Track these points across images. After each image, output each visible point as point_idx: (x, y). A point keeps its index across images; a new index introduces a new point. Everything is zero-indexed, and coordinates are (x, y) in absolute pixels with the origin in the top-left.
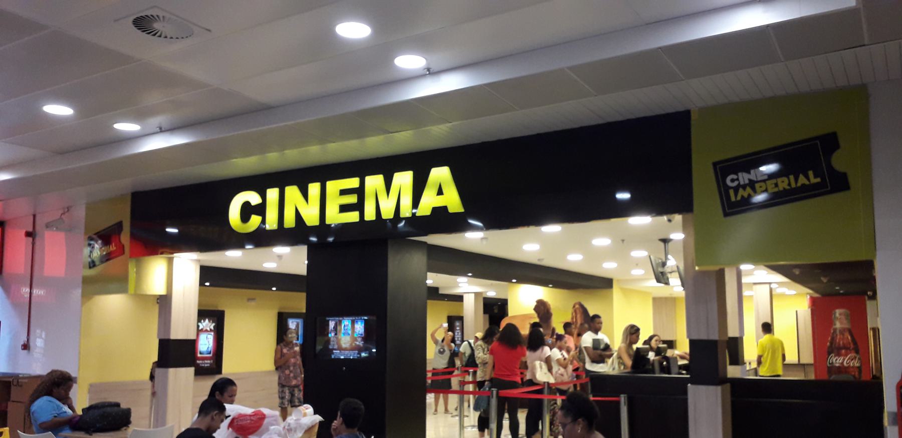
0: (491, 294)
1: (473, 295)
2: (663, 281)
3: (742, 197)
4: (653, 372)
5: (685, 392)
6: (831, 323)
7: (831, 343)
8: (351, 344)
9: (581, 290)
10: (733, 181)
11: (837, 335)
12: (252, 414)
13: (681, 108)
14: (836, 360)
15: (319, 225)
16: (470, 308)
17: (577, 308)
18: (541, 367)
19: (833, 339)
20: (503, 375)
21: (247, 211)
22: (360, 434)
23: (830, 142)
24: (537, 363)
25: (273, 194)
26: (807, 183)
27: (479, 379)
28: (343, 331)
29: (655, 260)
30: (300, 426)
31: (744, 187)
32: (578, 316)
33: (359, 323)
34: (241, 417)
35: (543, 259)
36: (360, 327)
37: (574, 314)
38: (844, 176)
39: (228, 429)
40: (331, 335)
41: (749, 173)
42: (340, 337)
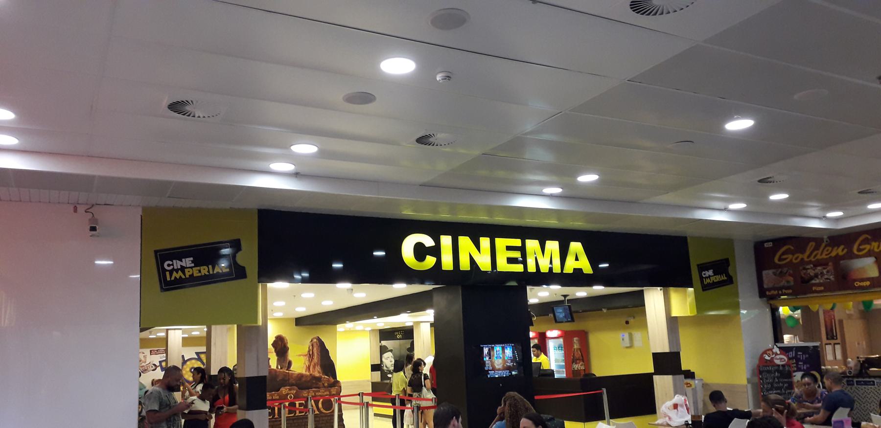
3: (175, 277)
8: (503, 366)
10: (169, 265)
13: (683, 235)
15: (879, 276)
21: (420, 251)
28: (495, 356)
31: (177, 271)
32: (315, 349)
33: (508, 349)
36: (509, 352)
37: (311, 348)
38: (243, 268)
40: (486, 359)
41: (181, 266)
42: (493, 360)
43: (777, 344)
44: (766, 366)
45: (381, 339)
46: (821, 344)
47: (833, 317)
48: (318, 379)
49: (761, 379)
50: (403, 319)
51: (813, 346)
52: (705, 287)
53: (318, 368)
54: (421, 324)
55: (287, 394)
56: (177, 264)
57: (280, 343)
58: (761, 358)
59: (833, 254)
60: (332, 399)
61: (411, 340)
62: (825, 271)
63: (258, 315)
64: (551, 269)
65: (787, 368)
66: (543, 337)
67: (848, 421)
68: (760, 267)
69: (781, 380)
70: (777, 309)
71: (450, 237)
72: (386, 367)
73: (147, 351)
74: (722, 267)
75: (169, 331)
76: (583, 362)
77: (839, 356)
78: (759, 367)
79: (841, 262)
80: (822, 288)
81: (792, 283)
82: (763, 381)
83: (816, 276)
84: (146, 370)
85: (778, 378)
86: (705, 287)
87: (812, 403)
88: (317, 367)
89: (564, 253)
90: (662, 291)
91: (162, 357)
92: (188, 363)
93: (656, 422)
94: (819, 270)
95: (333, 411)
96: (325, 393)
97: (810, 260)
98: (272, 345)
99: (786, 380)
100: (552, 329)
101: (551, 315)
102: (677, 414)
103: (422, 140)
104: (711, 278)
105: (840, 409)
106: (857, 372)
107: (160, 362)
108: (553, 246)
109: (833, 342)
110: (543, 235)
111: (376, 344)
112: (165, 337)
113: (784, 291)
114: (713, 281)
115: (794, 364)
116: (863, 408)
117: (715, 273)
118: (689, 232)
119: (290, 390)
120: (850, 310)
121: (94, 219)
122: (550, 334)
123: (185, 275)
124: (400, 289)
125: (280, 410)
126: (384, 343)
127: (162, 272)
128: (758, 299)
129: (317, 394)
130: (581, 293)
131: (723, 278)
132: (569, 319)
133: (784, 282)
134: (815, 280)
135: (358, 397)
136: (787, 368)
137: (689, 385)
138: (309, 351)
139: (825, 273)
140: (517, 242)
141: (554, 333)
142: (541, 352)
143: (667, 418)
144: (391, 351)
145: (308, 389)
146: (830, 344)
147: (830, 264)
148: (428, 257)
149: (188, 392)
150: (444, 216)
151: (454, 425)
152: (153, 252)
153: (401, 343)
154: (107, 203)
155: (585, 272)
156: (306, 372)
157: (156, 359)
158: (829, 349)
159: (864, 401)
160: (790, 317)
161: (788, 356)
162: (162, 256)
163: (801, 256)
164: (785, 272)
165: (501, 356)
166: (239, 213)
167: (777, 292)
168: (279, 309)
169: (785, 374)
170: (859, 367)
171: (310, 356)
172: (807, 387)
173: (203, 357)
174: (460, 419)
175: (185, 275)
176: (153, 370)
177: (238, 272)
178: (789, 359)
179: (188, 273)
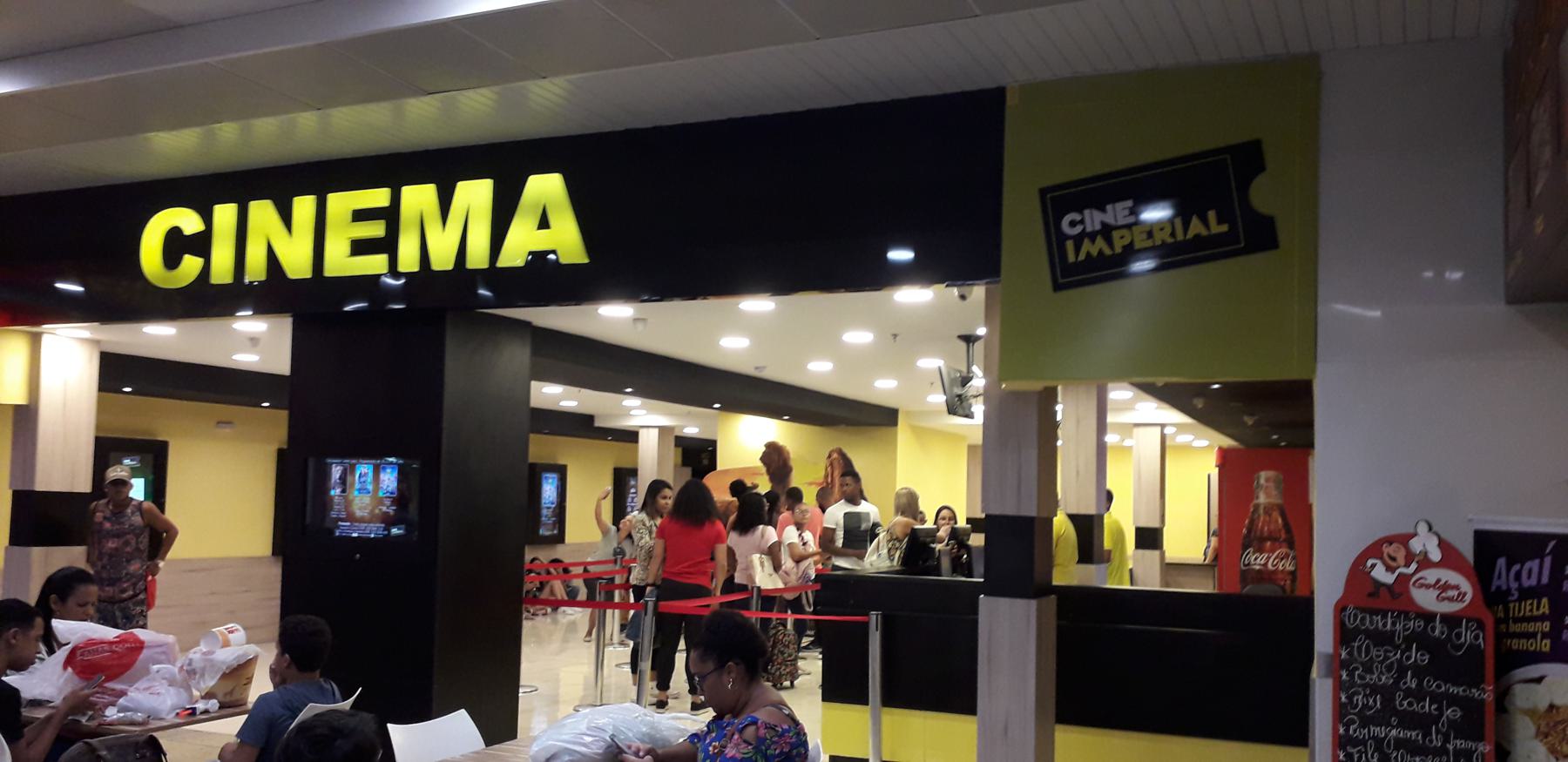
0: (691, 431)
1: (657, 430)
2: (961, 412)
3: (1088, 254)
4: (937, 570)
5: (974, 609)
6: (1251, 494)
7: (1249, 531)
8: (372, 511)
9: (843, 427)
10: (1073, 224)
11: (1259, 516)
12: (115, 640)
13: (989, 84)
14: (1256, 559)
16: (652, 459)
18: (762, 564)
19: (1252, 522)
20: (680, 574)
21: (176, 246)
22: (325, 681)
23: (1249, 158)
24: (756, 558)
25: (225, 214)
26: (1204, 232)
27: (633, 581)
28: (357, 486)
29: (949, 374)
30: (212, 664)
31: (1092, 237)
33: (389, 470)
34: (91, 644)
35: (764, 367)
36: (389, 479)
39: (65, 668)
40: (335, 492)
41: (1103, 210)
42: (351, 497)
56: (1093, 219)
69: (1433, 685)
78: (1344, 609)
82: (1351, 674)
85: (1419, 672)
98: (761, 459)
99: (1453, 690)
115: (1542, 618)
140: (378, 197)
165: (370, 487)
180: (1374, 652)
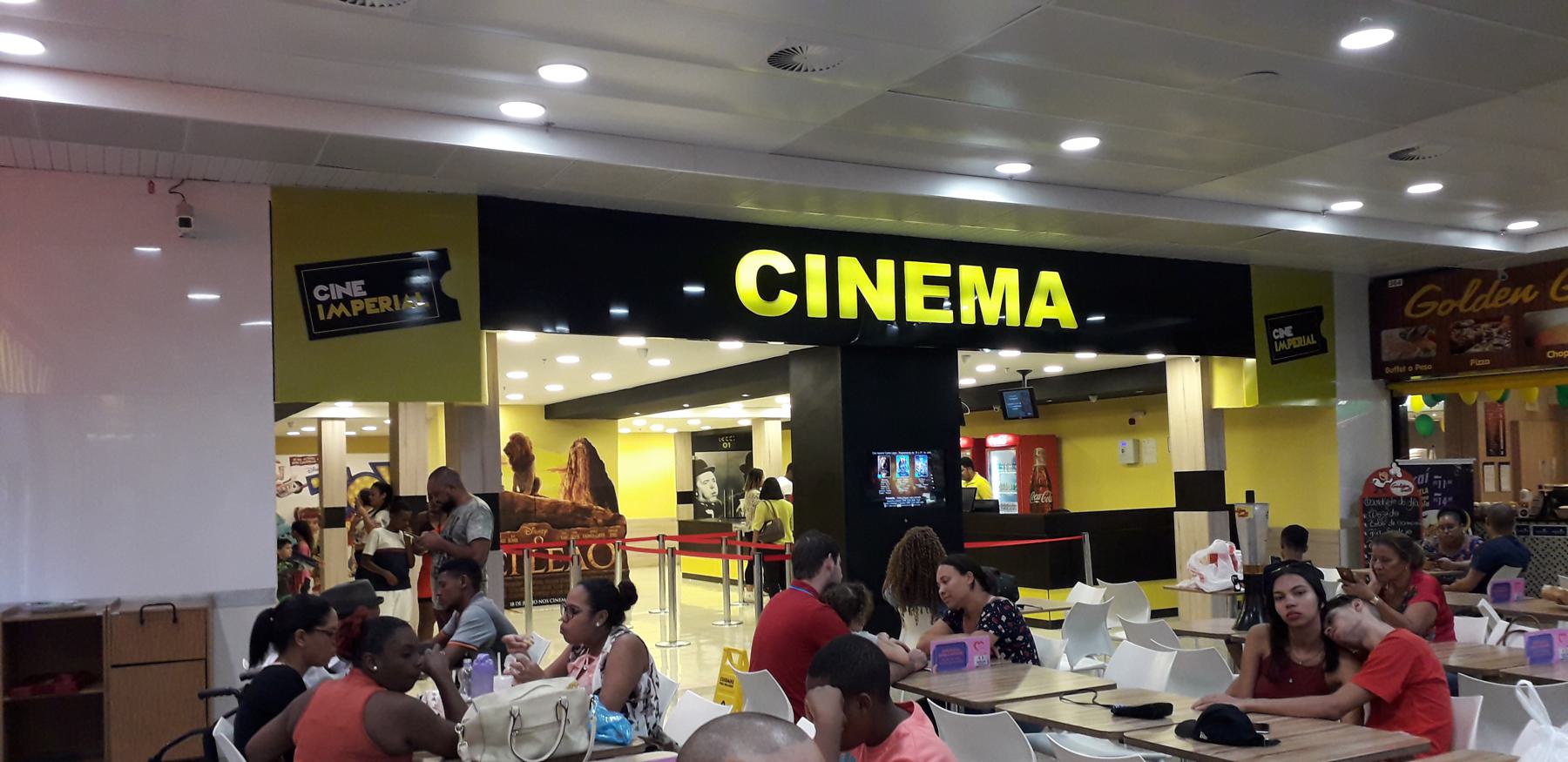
3: (334, 315)
8: (911, 488)
10: (322, 293)
17: (579, 448)
19: (1034, 477)
21: (769, 283)
28: (898, 471)
31: (336, 303)
32: (580, 460)
33: (921, 459)
36: (922, 464)
37: (573, 457)
38: (454, 303)
41: (344, 286)
42: (894, 479)
43: (1397, 460)
44: (1376, 499)
45: (695, 449)
46: (1477, 463)
47: (1501, 416)
48: (588, 511)
49: (1365, 521)
50: (732, 413)
51: (1463, 466)
52: (1278, 357)
53: (586, 493)
54: (766, 422)
55: (533, 536)
56: (337, 291)
57: (519, 449)
58: (1369, 483)
59: (1513, 300)
60: (611, 546)
61: (748, 452)
62: (1495, 331)
63: (483, 394)
64: (1002, 322)
65: (1412, 503)
66: (980, 447)
67: (1518, 583)
68: (1378, 322)
70: (1403, 400)
71: (822, 258)
72: (704, 496)
73: (284, 459)
74: (1309, 321)
75: (323, 422)
76: (1050, 490)
77: (1506, 486)
78: (1364, 499)
79: (1527, 314)
80: (1488, 362)
81: (1433, 353)
83: (1479, 339)
84: (284, 492)
85: (1395, 519)
86: (1278, 357)
87: (1454, 559)
88: (583, 491)
89: (1027, 290)
90: (1199, 363)
91: (312, 469)
92: (358, 481)
93: (1178, 586)
94: (1484, 329)
95: (614, 566)
96: (599, 536)
97: (1470, 312)
100: (996, 434)
101: (997, 408)
102: (1216, 570)
103: (780, 60)
104: (1289, 340)
105: (1505, 569)
106: (1537, 512)
107: (309, 479)
108: (1008, 277)
109: (1497, 459)
110: (990, 257)
111: (687, 458)
112: (316, 434)
113: (1418, 367)
114: (1292, 347)
115: (1426, 495)
116: (1542, 575)
117: (1296, 333)
118: (1254, 255)
119: (537, 528)
120: (1532, 405)
121: (184, 206)
122: (992, 441)
123: (351, 313)
124: (732, 351)
125: (520, 560)
126: (699, 456)
127: (310, 304)
128: (1370, 381)
129: (586, 536)
130: (1053, 366)
131: (1309, 342)
132: (1029, 414)
133: (1419, 350)
134: (1476, 348)
135: (657, 542)
136: (1412, 503)
137: (1243, 513)
138: (570, 464)
139: (1495, 335)
140: (944, 270)
141: (1001, 440)
142: (974, 470)
143: (1198, 578)
144: (712, 469)
145: (569, 527)
146: (1492, 463)
147: (1506, 318)
148: (783, 293)
149: (362, 522)
150: (813, 217)
151: (829, 568)
152: (294, 269)
153: (729, 457)
154: (206, 178)
155: (1063, 326)
156: (565, 498)
157: (302, 473)
158: (1489, 471)
159: (1544, 562)
160: (1424, 417)
161: (1415, 483)
162: (310, 276)
163: (1453, 304)
164: (1422, 332)
165: (908, 471)
166: (444, 201)
167: (1404, 368)
168: (517, 386)
169: (1408, 513)
170: (1540, 505)
171: (572, 471)
172: (1446, 530)
173: (384, 471)
174: (839, 559)
175: (351, 311)
176: (297, 492)
177: (444, 309)
178: (1418, 487)
179: (357, 307)
180: (1377, 514)
